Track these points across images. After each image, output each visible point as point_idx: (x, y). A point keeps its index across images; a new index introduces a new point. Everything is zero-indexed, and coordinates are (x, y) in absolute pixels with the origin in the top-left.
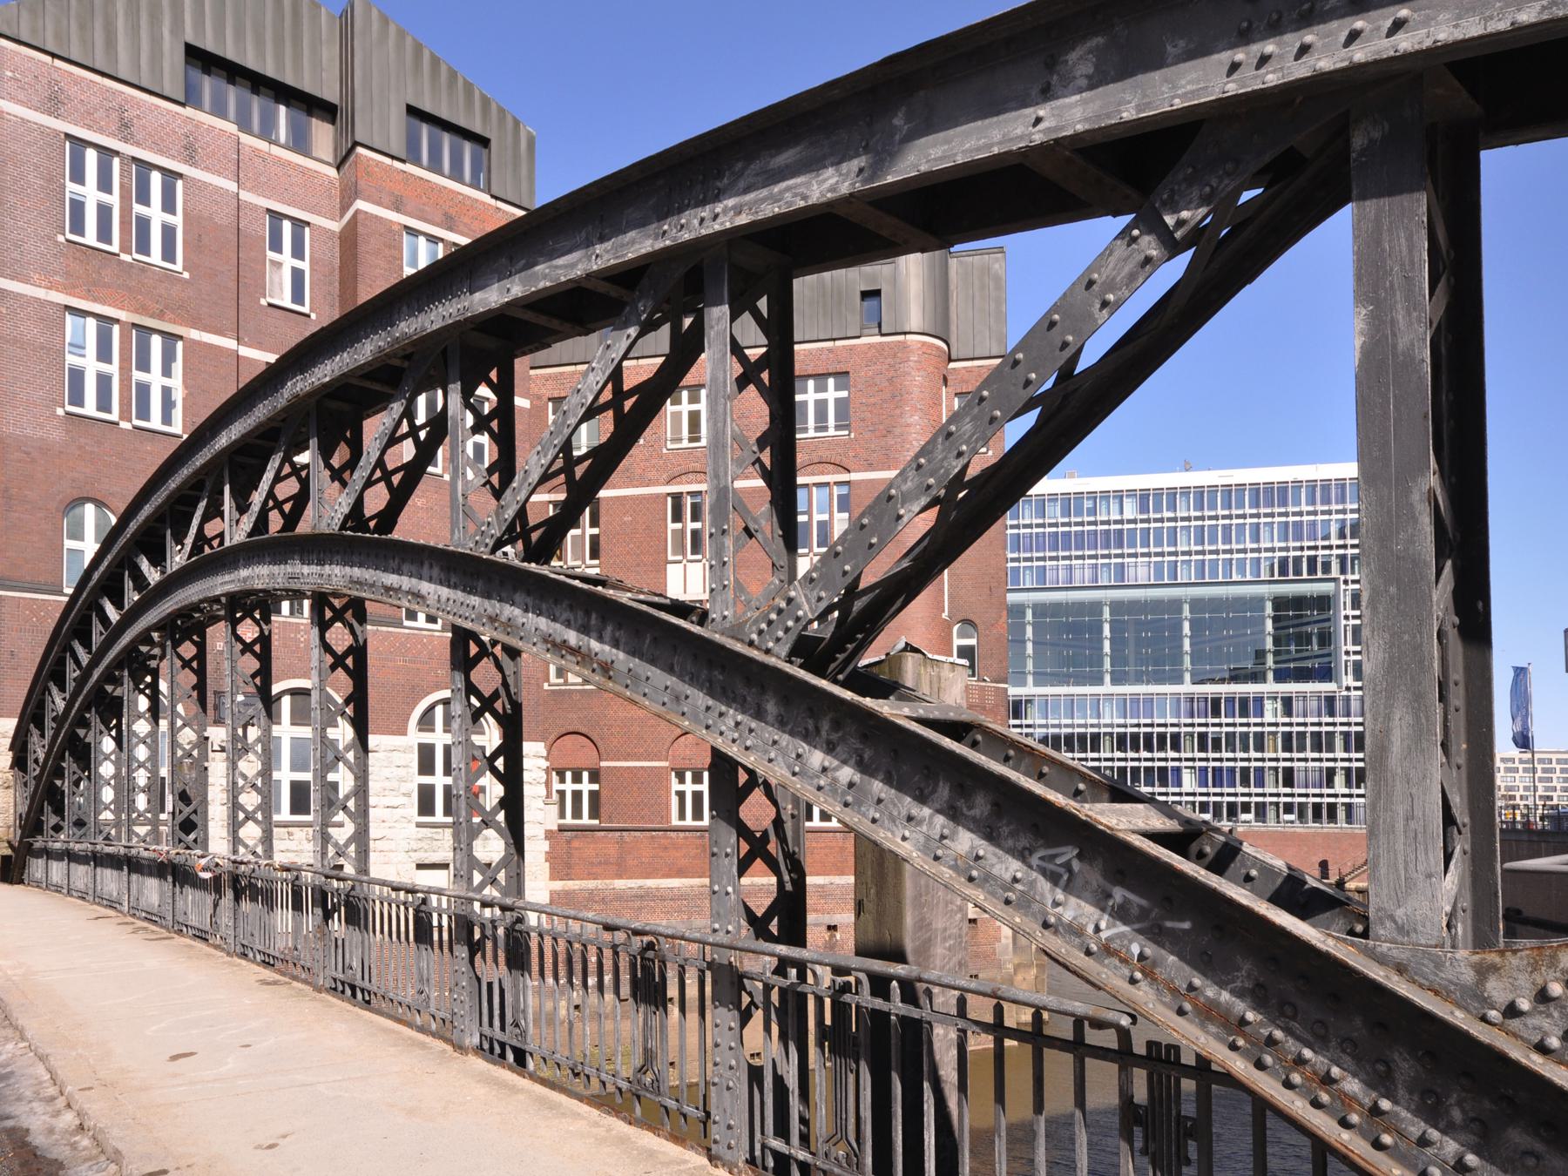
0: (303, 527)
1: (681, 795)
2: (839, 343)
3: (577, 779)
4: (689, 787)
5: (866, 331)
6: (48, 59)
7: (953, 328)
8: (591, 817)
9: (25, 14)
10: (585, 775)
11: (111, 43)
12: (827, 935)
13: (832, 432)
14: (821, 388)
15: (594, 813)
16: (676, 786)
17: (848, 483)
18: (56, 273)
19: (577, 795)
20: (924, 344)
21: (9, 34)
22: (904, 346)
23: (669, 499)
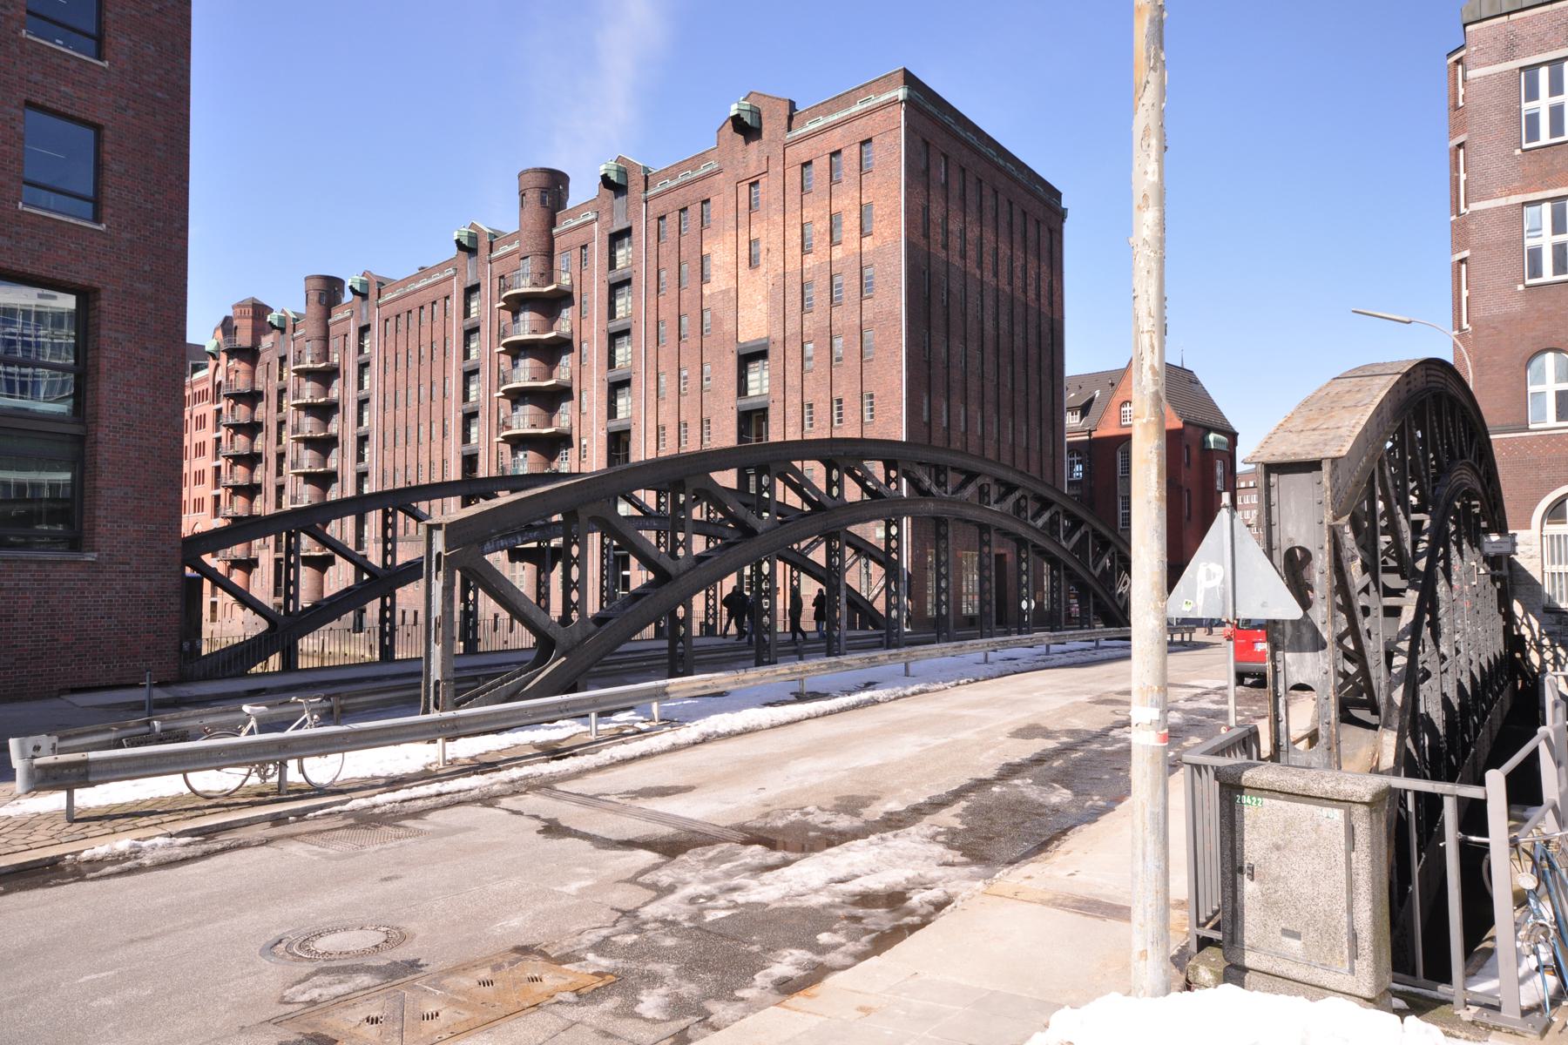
0: (704, 592)
6: (1506, 18)
18: (1513, 181)
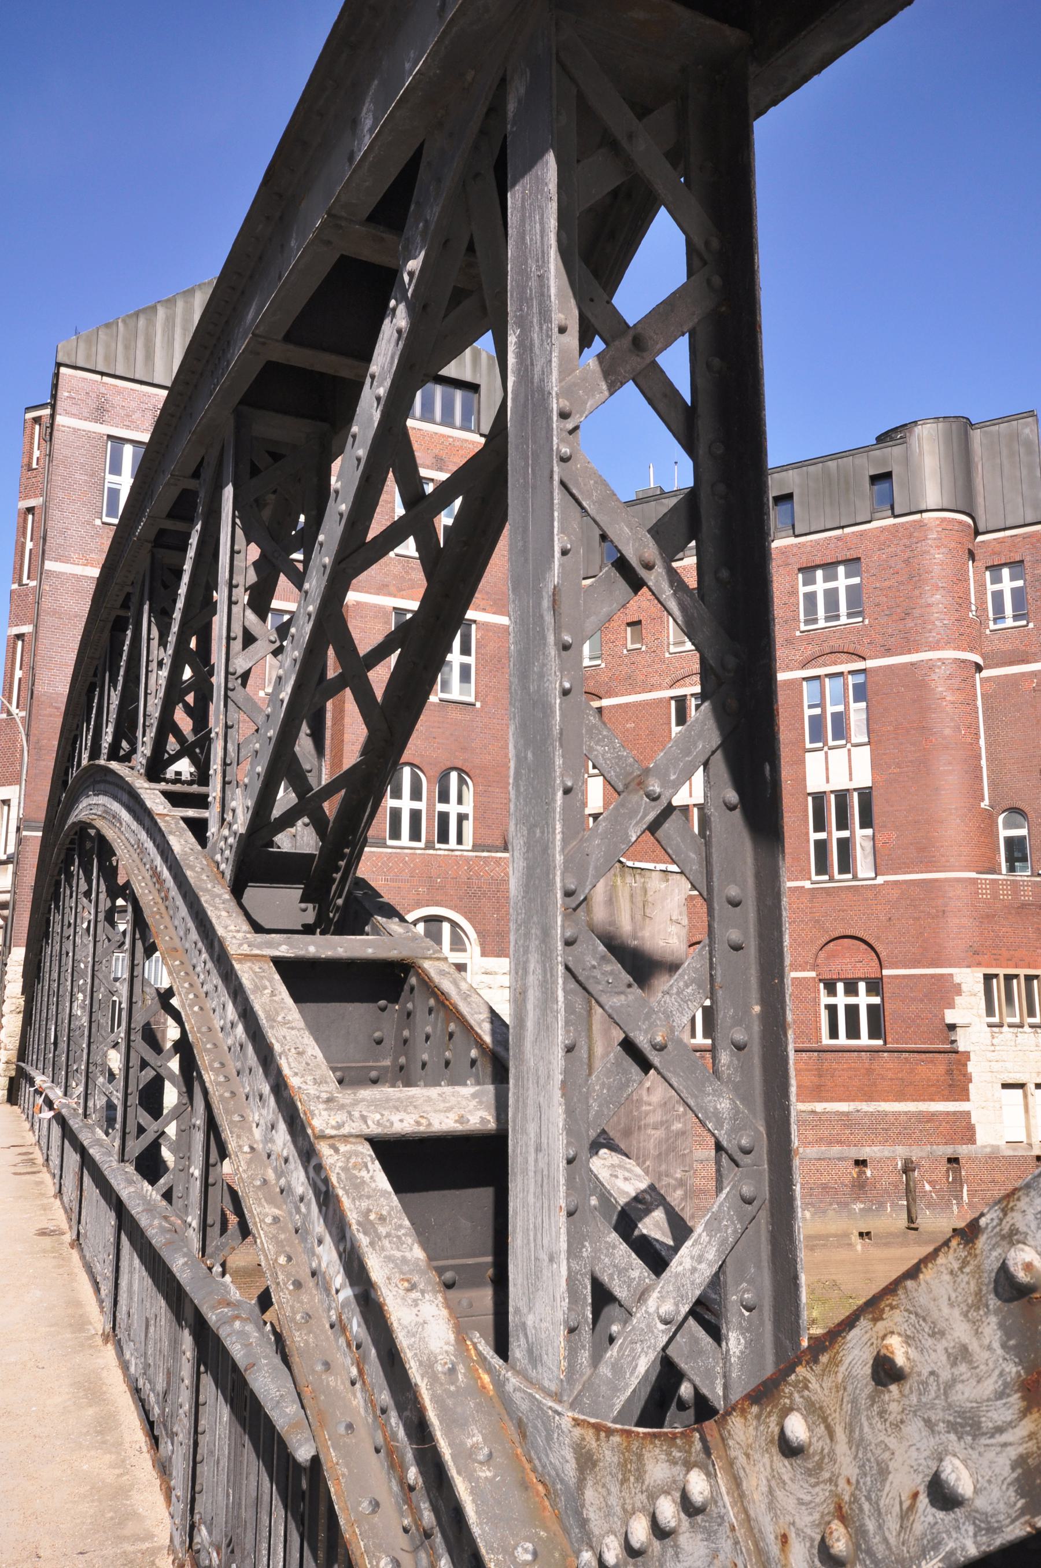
1: (832, 1009)
2: (847, 530)
3: (851, 989)
4: (841, 1000)
5: (877, 515)
6: (98, 377)
7: (980, 500)
8: (871, 1036)
9: (82, 346)
10: (862, 986)
11: (149, 356)
12: (854, 1172)
13: (844, 620)
14: (831, 577)
15: (875, 1031)
16: (825, 1000)
17: (863, 671)
19: (852, 1011)
20: (943, 520)
21: (68, 363)
22: (921, 525)
23: (673, 703)
